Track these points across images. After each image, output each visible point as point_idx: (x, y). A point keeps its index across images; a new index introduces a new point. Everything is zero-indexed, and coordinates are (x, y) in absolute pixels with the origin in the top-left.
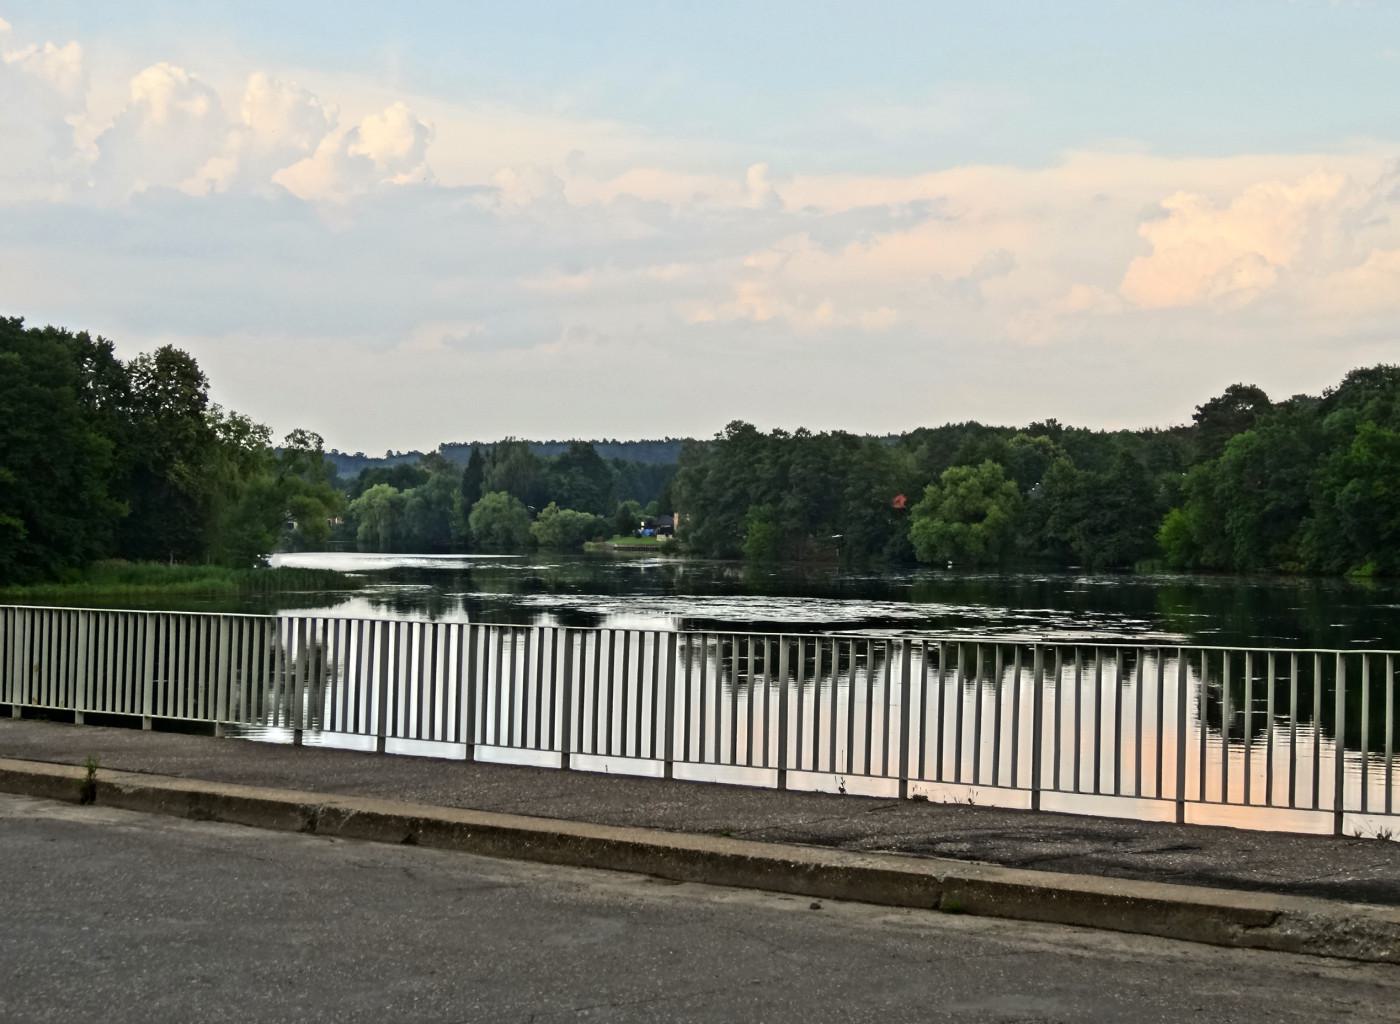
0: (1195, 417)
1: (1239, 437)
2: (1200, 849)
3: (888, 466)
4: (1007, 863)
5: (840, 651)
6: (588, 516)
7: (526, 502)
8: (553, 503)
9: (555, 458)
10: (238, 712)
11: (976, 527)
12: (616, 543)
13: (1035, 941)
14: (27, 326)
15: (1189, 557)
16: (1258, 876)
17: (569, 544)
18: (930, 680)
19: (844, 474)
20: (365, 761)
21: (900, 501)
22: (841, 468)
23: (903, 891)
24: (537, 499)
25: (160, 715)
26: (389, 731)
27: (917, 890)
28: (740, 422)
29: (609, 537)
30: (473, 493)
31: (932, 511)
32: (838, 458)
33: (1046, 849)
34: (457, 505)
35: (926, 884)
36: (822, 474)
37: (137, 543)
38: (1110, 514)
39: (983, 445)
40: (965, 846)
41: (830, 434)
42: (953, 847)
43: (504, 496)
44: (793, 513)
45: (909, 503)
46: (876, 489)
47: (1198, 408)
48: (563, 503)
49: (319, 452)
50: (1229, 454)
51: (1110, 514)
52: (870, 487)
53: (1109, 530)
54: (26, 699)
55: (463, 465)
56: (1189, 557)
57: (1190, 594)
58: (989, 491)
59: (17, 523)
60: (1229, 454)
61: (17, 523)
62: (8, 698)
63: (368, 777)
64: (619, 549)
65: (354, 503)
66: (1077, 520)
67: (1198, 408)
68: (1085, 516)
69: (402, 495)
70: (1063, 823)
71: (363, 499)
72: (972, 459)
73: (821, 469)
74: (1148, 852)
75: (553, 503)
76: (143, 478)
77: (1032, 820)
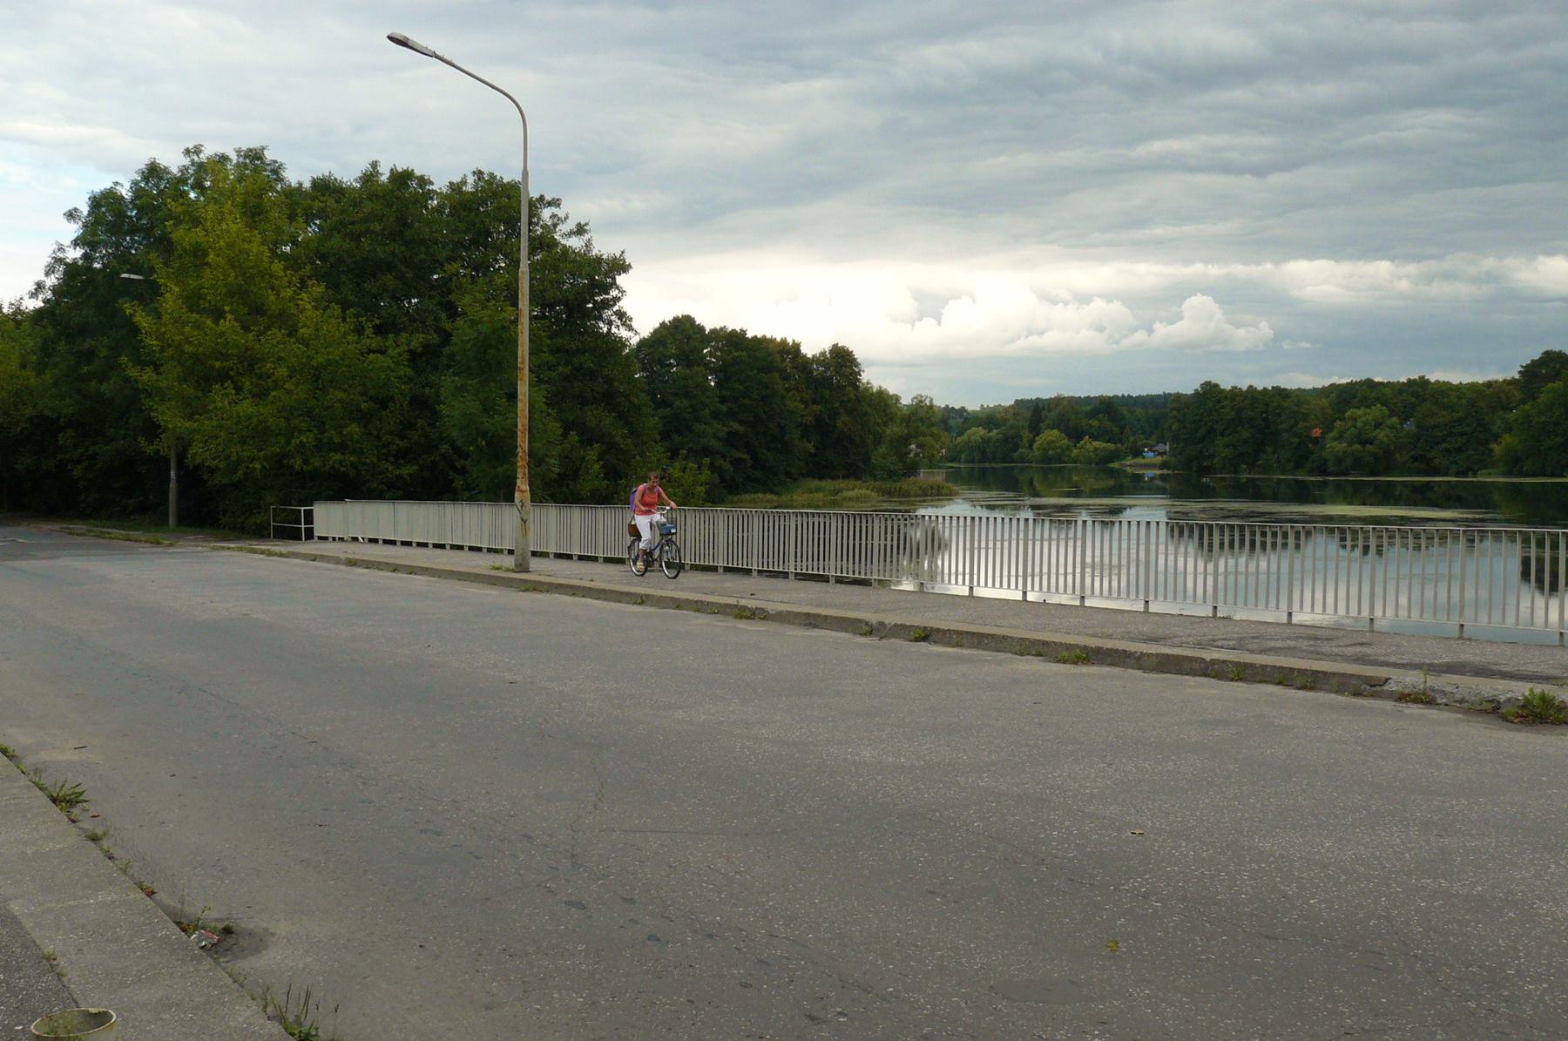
0: (1520, 372)
1: (1550, 385)
2: (1370, 644)
3: (1308, 409)
4: (1251, 651)
5: (1251, 535)
6: (1111, 446)
7: (1070, 437)
8: (1087, 437)
9: (1088, 408)
10: (842, 569)
11: (1369, 447)
12: (1129, 461)
13: (706, 581)
14: (749, 335)
15: (1514, 464)
16: (1393, 659)
17: (1102, 463)
18: (1170, 547)
19: (1279, 415)
20: (910, 597)
21: (1317, 432)
22: (1277, 411)
23: (1187, 666)
24: (1076, 435)
25: (839, 574)
26: (975, 583)
27: (1196, 666)
28: (1210, 382)
29: (1124, 458)
30: (1035, 429)
31: (1340, 438)
32: (1275, 404)
33: (1279, 644)
34: (1025, 440)
35: (1200, 663)
36: (1264, 415)
37: (820, 469)
38: (1461, 440)
39: (1373, 395)
40: (1231, 643)
41: (1270, 388)
42: (1225, 643)
43: (1056, 432)
44: (1246, 441)
45: (1324, 433)
46: (1302, 424)
47: (1522, 367)
48: (1095, 438)
49: (931, 407)
50: (1544, 398)
51: (1461, 440)
52: (1297, 424)
53: (1459, 451)
54: (726, 562)
55: (1028, 415)
56: (1514, 464)
57: (1515, 491)
58: (1378, 425)
59: (745, 456)
60: (1544, 398)
61: (745, 456)
62: (716, 561)
63: (908, 605)
64: (1131, 466)
65: (959, 439)
66: (1437, 443)
67: (1522, 367)
68: (1444, 441)
69: (990, 434)
70: (1302, 630)
71: (965, 437)
72: (1366, 402)
73: (1263, 413)
74: (1346, 646)
75: (1087, 437)
76: (822, 429)
77: (1289, 630)
